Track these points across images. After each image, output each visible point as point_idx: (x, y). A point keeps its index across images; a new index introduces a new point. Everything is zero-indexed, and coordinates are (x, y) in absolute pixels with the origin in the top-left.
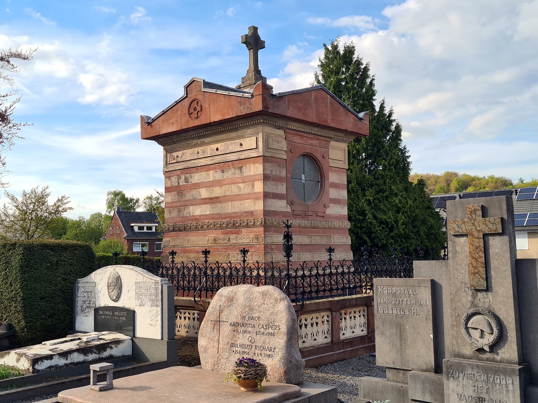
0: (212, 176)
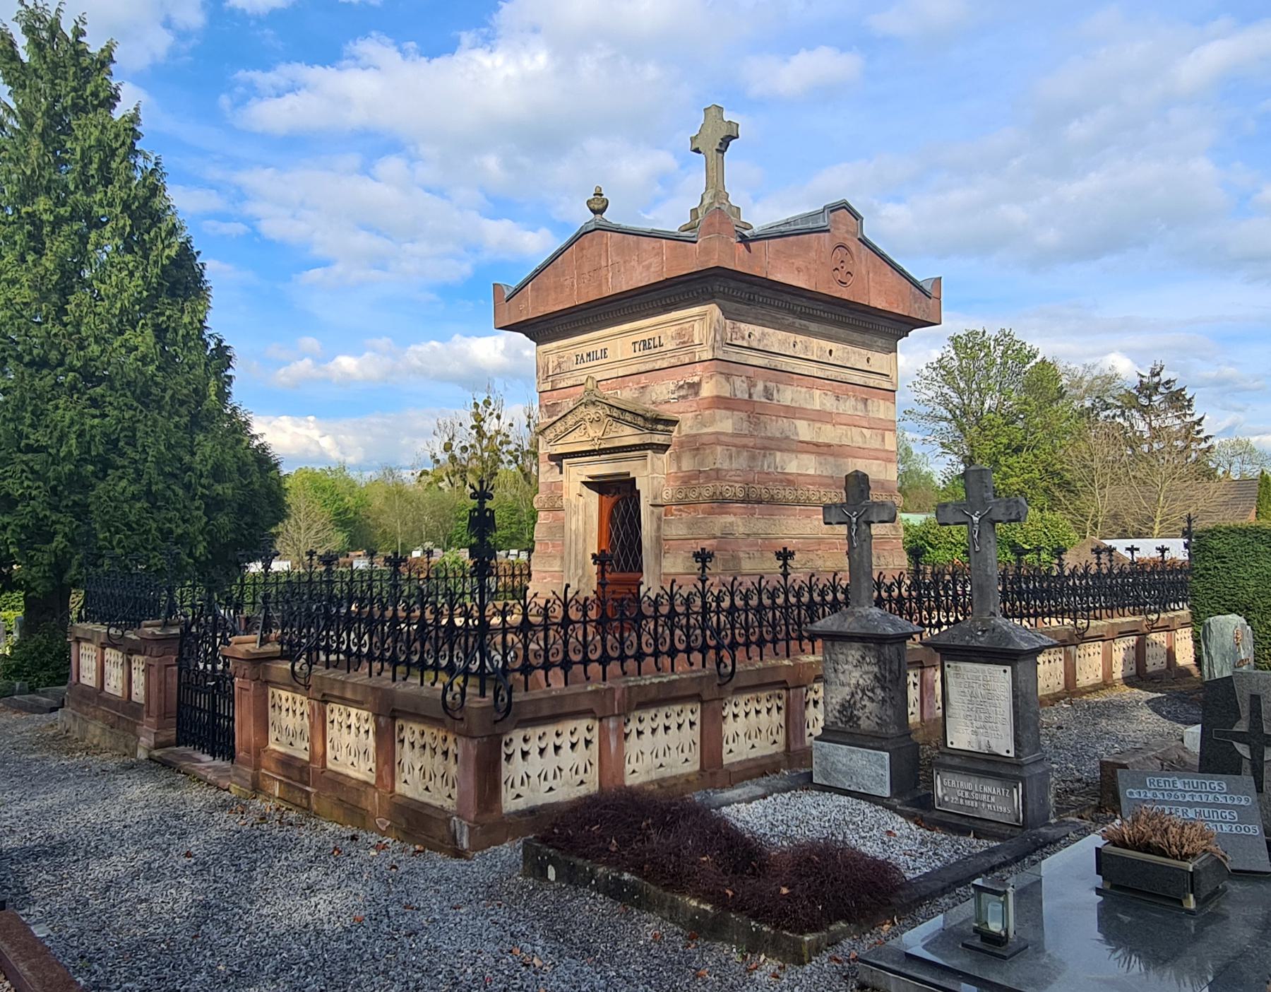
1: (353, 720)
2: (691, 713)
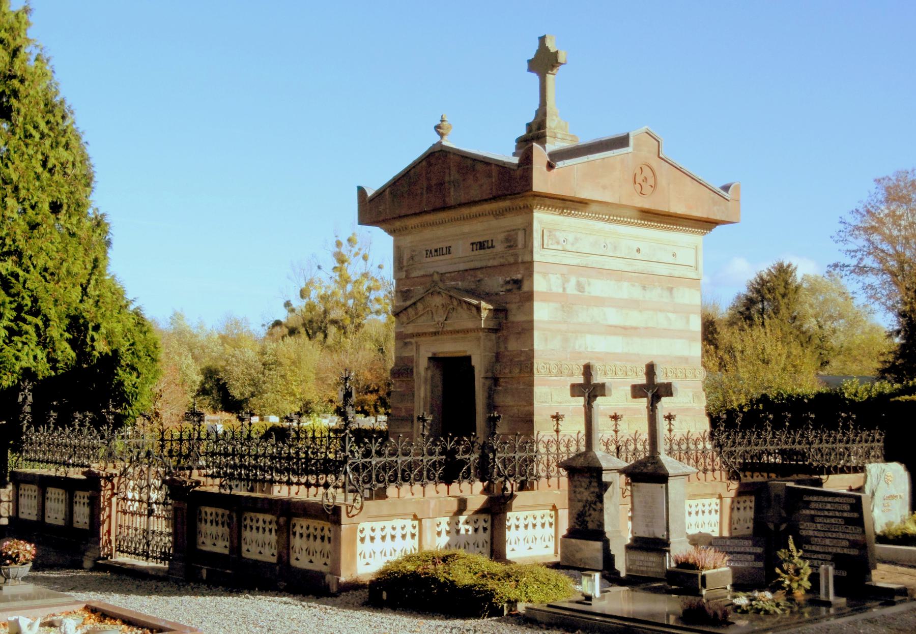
0: (626, 290)
1: (261, 524)
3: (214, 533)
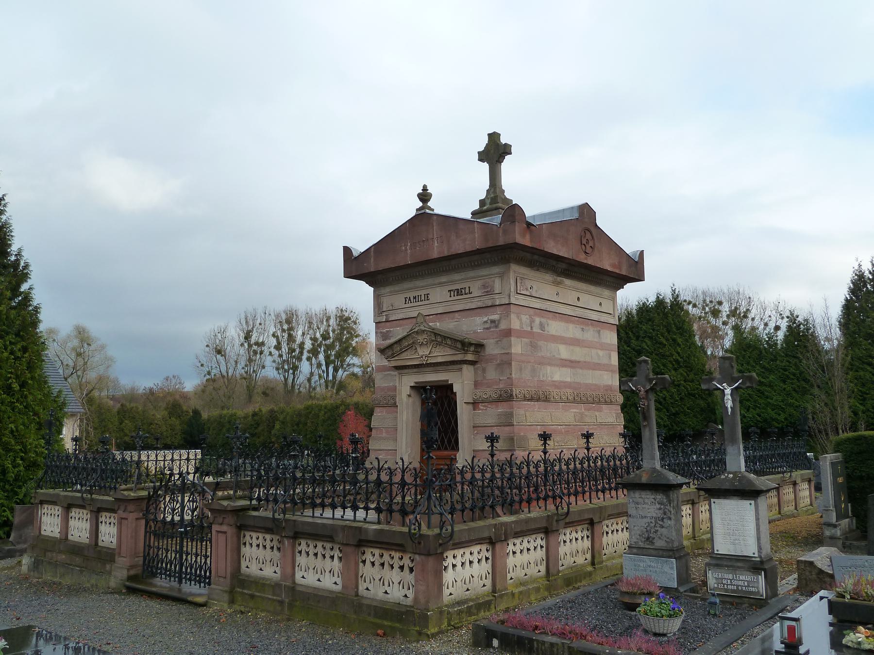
0: (572, 331)
2: (538, 540)
3: (261, 558)
